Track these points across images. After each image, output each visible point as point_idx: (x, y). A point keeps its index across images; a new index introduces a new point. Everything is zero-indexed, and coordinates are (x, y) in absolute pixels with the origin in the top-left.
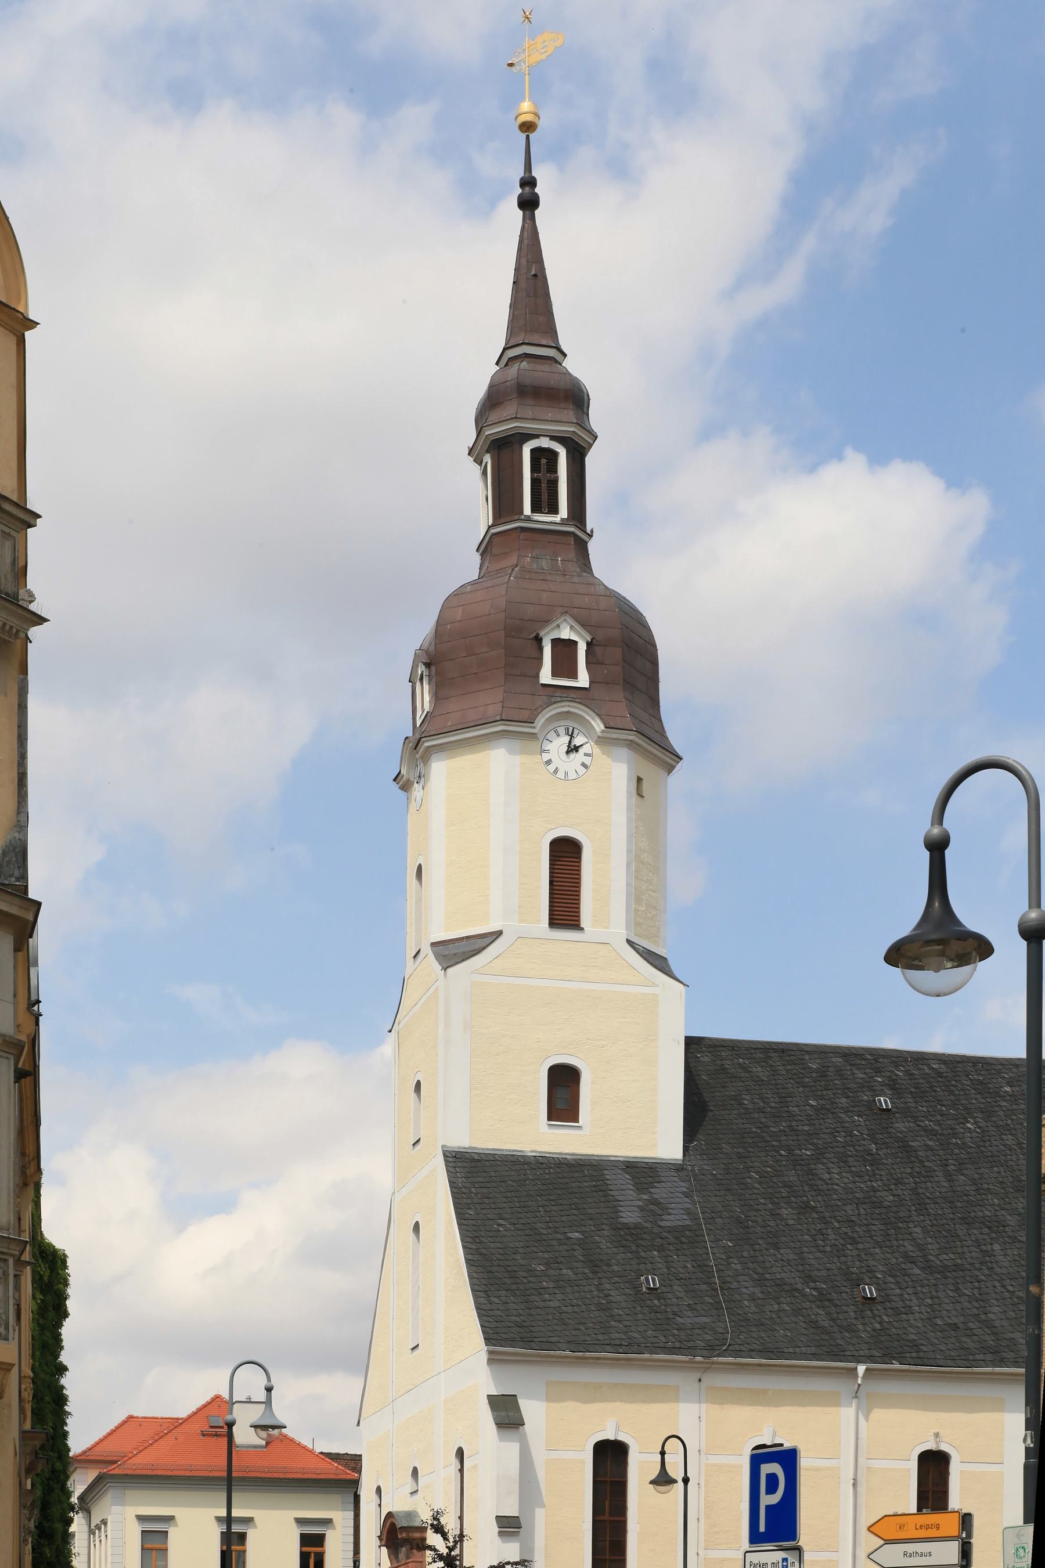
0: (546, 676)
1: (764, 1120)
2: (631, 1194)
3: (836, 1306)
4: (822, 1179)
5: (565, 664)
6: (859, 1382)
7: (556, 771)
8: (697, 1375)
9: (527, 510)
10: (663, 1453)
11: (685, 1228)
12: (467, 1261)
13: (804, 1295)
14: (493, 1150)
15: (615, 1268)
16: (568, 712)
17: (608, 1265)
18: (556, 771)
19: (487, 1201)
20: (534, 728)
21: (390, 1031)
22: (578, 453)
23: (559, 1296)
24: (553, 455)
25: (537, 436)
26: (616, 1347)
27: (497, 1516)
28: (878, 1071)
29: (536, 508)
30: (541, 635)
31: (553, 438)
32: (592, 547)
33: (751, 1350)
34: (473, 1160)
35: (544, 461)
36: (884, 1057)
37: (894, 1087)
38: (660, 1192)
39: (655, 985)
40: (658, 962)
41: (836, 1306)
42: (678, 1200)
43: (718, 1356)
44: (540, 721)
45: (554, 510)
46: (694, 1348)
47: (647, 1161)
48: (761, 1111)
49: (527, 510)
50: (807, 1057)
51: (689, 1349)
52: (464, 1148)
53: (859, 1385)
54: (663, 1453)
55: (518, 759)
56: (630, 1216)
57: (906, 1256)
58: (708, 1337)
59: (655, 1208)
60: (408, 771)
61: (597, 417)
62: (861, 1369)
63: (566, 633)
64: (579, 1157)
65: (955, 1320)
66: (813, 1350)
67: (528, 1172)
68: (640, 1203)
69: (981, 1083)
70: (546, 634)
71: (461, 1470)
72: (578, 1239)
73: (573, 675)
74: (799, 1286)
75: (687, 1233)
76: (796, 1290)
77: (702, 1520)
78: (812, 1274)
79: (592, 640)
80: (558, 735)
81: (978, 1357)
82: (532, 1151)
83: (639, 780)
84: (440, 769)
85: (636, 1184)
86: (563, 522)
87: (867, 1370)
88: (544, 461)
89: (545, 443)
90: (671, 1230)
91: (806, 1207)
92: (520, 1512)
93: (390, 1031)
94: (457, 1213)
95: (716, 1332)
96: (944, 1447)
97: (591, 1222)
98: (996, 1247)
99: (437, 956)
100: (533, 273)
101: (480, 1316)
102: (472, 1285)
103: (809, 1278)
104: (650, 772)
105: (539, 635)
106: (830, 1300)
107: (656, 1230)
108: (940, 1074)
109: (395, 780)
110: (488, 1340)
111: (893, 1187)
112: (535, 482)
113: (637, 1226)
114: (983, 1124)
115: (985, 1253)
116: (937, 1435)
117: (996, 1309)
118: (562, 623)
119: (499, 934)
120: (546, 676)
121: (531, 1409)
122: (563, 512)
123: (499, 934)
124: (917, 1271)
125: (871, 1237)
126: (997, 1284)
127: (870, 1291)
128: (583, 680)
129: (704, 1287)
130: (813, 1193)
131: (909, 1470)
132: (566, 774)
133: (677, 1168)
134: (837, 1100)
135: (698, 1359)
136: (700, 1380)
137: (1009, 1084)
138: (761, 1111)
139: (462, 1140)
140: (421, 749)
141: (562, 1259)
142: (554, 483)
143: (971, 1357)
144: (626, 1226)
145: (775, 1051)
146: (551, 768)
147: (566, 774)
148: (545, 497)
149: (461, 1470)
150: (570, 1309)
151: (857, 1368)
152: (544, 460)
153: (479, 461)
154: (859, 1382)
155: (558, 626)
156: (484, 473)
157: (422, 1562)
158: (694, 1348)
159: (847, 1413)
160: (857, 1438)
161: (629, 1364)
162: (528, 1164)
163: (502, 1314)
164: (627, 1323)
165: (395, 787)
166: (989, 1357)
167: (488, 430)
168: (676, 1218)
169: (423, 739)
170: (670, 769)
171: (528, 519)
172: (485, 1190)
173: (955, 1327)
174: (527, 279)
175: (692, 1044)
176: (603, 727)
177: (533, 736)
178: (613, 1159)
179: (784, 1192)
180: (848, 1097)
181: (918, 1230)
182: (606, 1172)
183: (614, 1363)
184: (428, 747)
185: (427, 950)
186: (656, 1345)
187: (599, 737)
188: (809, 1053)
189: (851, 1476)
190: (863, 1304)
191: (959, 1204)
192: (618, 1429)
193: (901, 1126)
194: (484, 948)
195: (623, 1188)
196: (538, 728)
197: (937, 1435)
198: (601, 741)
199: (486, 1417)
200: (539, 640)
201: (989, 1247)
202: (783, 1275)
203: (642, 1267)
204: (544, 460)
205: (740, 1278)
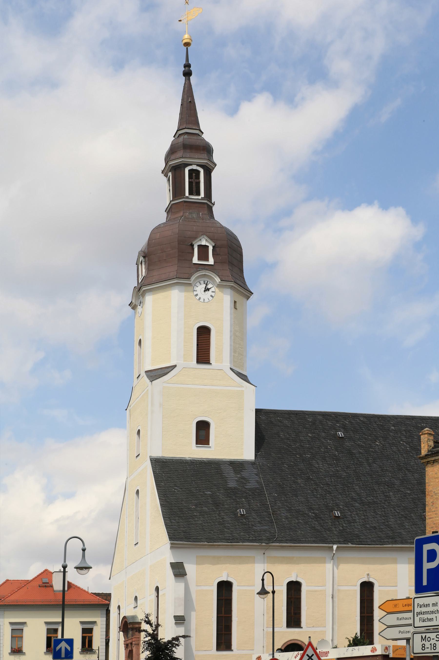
0: (195, 260)
1: (289, 443)
2: (232, 474)
3: (323, 520)
4: (315, 467)
5: (203, 254)
6: (334, 552)
7: (200, 299)
8: (263, 552)
9: (187, 194)
10: (263, 580)
11: (257, 488)
12: (161, 505)
13: (309, 516)
14: (172, 457)
15: (226, 506)
16: (205, 275)
17: (223, 505)
18: (200, 299)
19: (169, 479)
20: (190, 281)
21: (126, 410)
22: (208, 172)
23: (202, 519)
24: (198, 172)
25: (191, 165)
26: (227, 540)
27: (174, 616)
28: (337, 422)
29: (191, 193)
30: (193, 243)
31: (198, 165)
32: (214, 209)
33: (287, 540)
34: (163, 462)
35: (194, 174)
36: (340, 416)
37: (344, 428)
38: (245, 474)
39: (242, 387)
40: (244, 377)
41: (323, 520)
42: (254, 477)
43: (272, 543)
44: (193, 278)
45: (198, 194)
46: (262, 540)
47: (239, 461)
48: (288, 439)
49: (187, 194)
50: (307, 416)
51: (260, 541)
52: (160, 457)
53: (334, 554)
54: (263, 580)
55: (183, 294)
56: (232, 484)
57: (352, 498)
58: (267, 535)
59: (243, 481)
60: (135, 301)
61: (216, 157)
62: (335, 547)
63: (204, 243)
64: (209, 460)
65: (374, 525)
66: (314, 539)
67: (187, 466)
68: (237, 478)
69: (382, 426)
70: (196, 243)
71: (158, 596)
72: (209, 494)
73: (207, 260)
74: (307, 512)
75: (257, 491)
76: (306, 514)
77: (265, 615)
78: (312, 507)
79: (215, 245)
80: (201, 284)
81: (385, 540)
82: (189, 458)
83: (235, 302)
84: (149, 299)
85: (234, 471)
86: (202, 199)
87: (337, 547)
88: (194, 174)
89: (194, 167)
90: (250, 490)
91: (309, 478)
92: (184, 615)
93: (126, 410)
94: (156, 485)
95: (271, 533)
96: (371, 580)
97: (215, 487)
98: (391, 494)
99: (148, 376)
100: (189, 101)
101: (167, 528)
102: (163, 515)
103: (311, 509)
104: (240, 299)
105: (192, 243)
106: (320, 518)
107: (244, 490)
108: (364, 422)
109: (129, 305)
110: (170, 539)
111: (345, 469)
112: (190, 183)
113: (235, 488)
114: (383, 443)
115: (386, 496)
116: (368, 575)
117: (392, 520)
118: (202, 238)
119: (175, 366)
120: (195, 260)
121: (189, 568)
122: (202, 194)
123: (175, 366)
124: (357, 505)
125: (337, 490)
126: (392, 509)
127: (337, 513)
128: (211, 261)
129: (265, 513)
130: (311, 473)
131: (356, 590)
132: (204, 300)
133: (252, 463)
134: (320, 434)
135: (264, 544)
136: (264, 554)
137: (393, 426)
138: (288, 439)
139: (159, 453)
140: (141, 291)
141: (203, 503)
142: (198, 184)
143: (382, 541)
144: (231, 488)
145: (293, 414)
146: (198, 297)
147: (204, 300)
148: (194, 189)
149: (158, 596)
150: (206, 524)
151: (333, 546)
152: (194, 174)
153: (166, 175)
154: (334, 552)
155: (201, 240)
156: (169, 180)
157: (139, 638)
158: (262, 540)
159: (329, 566)
160: (333, 577)
161: (233, 547)
162: (188, 463)
163: (177, 527)
164: (232, 530)
165: (130, 308)
166: (390, 540)
167: (171, 162)
168: (252, 484)
169: (142, 287)
170: (248, 298)
171: (187, 198)
172: (168, 475)
173: (375, 528)
174: (187, 103)
175: (258, 412)
176: (220, 281)
177: (190, 284)
178: (224, 460)
179: (299, 472)
180: (325, 433)
181: (357, 487)
182: (221, 466)
183: (226, 547)
184: (144, 290)
185: (143, 374)
186: (245, 539)
187: (218, 285)
188: (307, 414)
189: (331, 594)
190: (334, 519)
191: (374, 476)
192: (228, 576)
193: (348, 444)
194: (168, 373)
195: (230, 473)
196: (192, 281)
197: (368, 575)
198: (219, 286)
199: (170, 572)
200: (192, 246)
201: (388, 494)
202: (300, 508)
203: (238, 505)
204: (194, 174)
205: (281, 509)
